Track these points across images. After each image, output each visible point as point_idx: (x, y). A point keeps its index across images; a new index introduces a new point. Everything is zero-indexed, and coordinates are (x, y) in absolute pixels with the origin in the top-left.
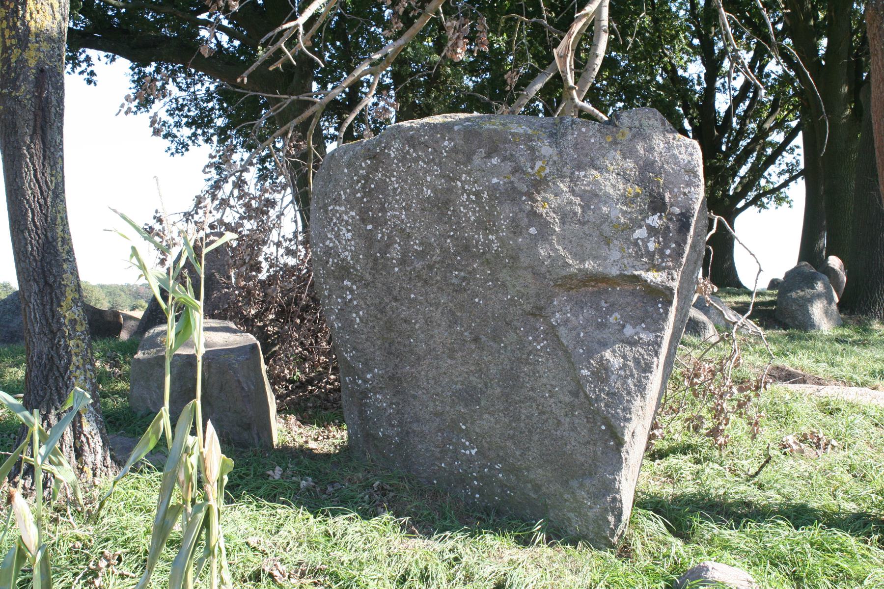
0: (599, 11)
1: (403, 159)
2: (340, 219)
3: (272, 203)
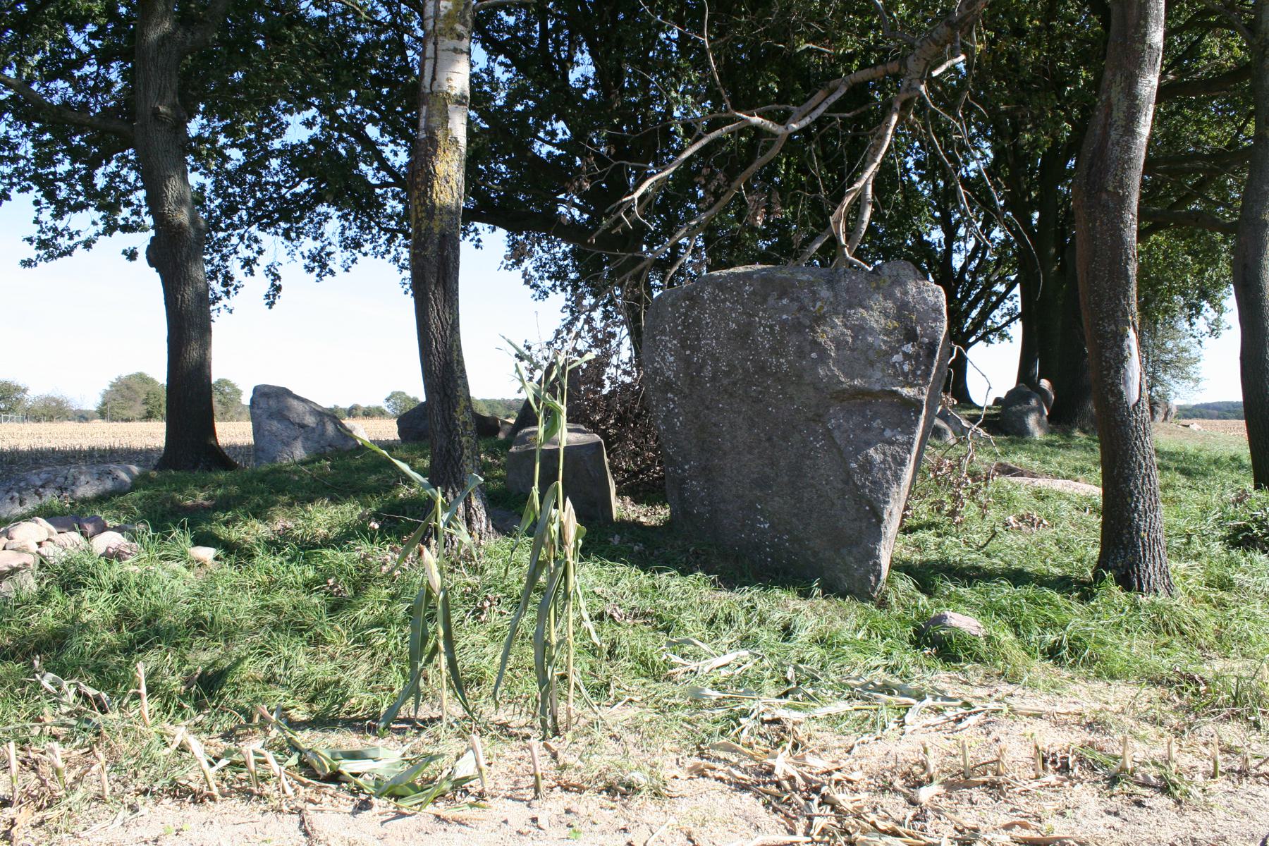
0: (864, 187)
1: (714, 301)
2: (666, 346)
3: (613, 335)
